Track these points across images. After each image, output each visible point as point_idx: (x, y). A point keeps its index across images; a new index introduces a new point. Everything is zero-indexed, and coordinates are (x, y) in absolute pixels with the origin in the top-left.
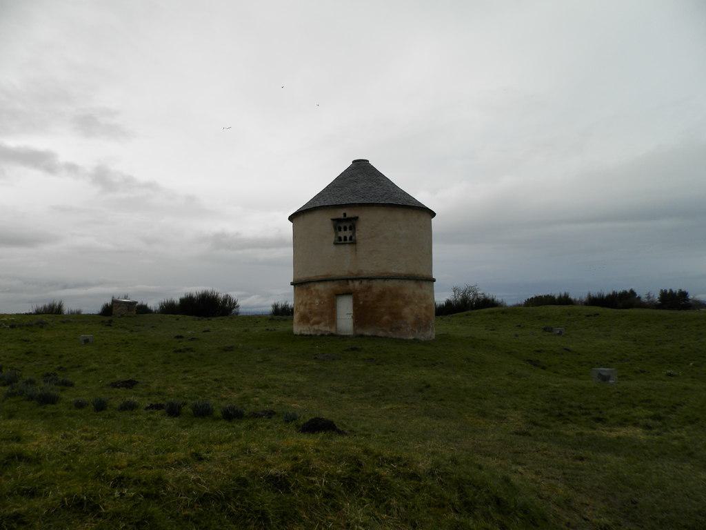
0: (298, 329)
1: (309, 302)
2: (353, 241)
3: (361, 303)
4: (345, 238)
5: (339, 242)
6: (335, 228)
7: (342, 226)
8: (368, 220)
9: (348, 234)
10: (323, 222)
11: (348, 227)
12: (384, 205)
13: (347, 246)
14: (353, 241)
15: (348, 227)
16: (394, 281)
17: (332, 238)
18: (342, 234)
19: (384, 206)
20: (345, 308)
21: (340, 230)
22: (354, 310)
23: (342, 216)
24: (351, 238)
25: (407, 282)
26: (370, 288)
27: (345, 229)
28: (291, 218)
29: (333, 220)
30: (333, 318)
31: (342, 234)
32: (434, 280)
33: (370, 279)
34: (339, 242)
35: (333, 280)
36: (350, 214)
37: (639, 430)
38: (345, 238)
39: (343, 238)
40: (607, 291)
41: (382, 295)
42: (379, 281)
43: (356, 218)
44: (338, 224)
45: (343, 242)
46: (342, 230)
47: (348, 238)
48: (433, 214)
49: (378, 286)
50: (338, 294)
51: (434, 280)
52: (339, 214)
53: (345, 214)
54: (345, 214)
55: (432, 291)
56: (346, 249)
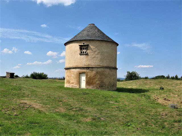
0: (66, 85)
1: (70, 75)
3: (89, 76)
5: (81, 54)
6: (80, 48)
7: (83, 48)
9: (85, 51)
10: (76, 46)
11: (85, 48)
12: (106, 41)
15: (85, 48)
16: (101, 69)
17: (79, 52)
20: (83, 78)
22: (86, 79)
24: (86, 52)
25: (106, 69)
27: (84, 49)
30: (79, 83)
32: (117, 69)
34: (81, 54)
35: (101, 68)
37: (102, 122)
40: (54, 77)
43: (88, 45)
44: (81, 47)
45: (83, 53)
46: (83, 49)
47: (85, 52)
48: (118, 45)
50: (80, 74)
51: (117, 69)
54: (84, 44)
55: (116, 73)
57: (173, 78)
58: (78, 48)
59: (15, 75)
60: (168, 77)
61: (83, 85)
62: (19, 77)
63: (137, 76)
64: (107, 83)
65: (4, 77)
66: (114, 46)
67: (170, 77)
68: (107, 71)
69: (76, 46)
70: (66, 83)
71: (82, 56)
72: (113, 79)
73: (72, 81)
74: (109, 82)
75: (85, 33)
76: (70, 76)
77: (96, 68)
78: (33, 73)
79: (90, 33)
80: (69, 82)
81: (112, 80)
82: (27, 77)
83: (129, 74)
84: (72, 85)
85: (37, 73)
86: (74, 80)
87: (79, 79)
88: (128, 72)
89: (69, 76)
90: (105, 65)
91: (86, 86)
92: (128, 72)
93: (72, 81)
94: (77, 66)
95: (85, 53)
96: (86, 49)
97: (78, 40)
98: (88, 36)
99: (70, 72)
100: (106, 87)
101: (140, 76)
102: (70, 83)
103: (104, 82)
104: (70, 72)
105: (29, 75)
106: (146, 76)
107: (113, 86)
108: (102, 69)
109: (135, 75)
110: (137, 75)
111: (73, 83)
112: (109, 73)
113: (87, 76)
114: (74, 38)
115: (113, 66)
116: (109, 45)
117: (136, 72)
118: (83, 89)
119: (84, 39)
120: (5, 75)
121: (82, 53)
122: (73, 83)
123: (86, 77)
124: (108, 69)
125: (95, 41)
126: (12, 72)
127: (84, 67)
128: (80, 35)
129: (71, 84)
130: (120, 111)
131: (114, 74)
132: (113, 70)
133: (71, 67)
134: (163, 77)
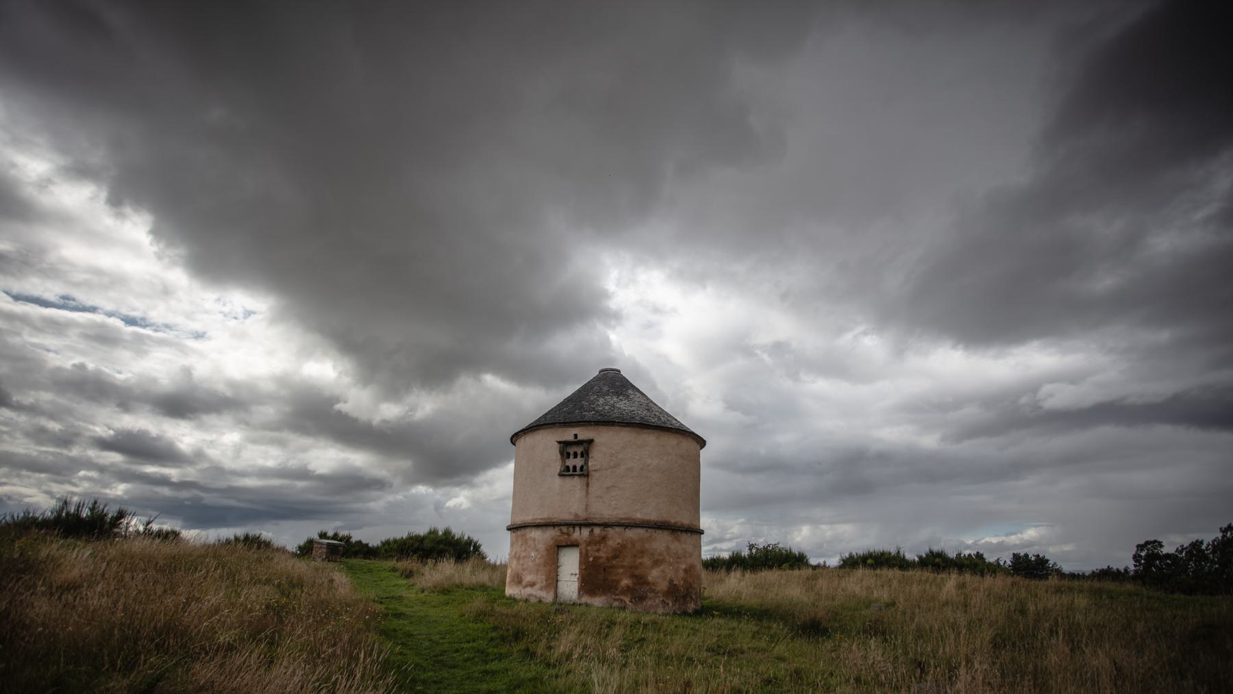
1: (523, 554)
2: (584, 473)
4: (575, 467)
5: (566, 472)
6: (562, 453)
7: (571, 450)
8: (608, 444)
9: (579, 462)
10: (548, 442)
14: (584, 473)
17: (557, 467)
18: (571, 462)
19: (595, 521)
20: (570, 563)
21: (568, 455)
23: (571, 438)
24: (582, 468)
25: (659, 532)
26: (604, 539)
27: (575, 455)
28: (512, 528)
29: (559, 442)
30: (553, 581)
31: (571, 462)
32: (702, 532)
33: (605, 525)
34: (566, 472)
36: (583, 434)
38: (575, 467)
41: (618, 553)
42: (618, 529)
43: (591, 442)
44: (565, 448)
48: (702, 443)
49: (615, 537)
51: (702, 532)
52: (568, 434)
53: (576, 436)
54: (576, 436)
56: (576, 483)
58: (554, 452)
61: (569, 585)
64: (663, 586)
66: (687, 444)
68: (661, 541)
69: (548, 442)
71: (568, 480)
73: (528, 578)
74: (671, 581)
77: (619, 525)
80: (518, 580)
84: (529, 590)
89: (519, 559)
90: (653, 516)
93: (528, 578)
99: (526, 542)
103: (648, 584)
104: (526, 542)
108: (640, 532)
111: (532, 585)
112: (668, 547)
122: (532, 585)
124: (666, 533)
125: (616, 428)
130: (655, 623)
131: (690, 548)
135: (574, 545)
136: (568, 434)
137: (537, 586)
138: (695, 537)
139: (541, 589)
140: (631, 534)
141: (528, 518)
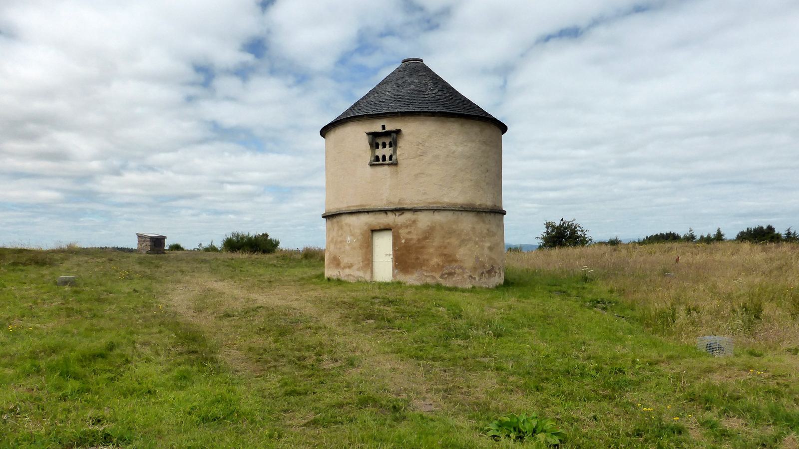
1: (339, 239)
3: (403, 241)
4: (384, 157)
5: (376, 162)
6: (371, 145)
7: (380, 141)
9: (387, 151)
10: (356, 136)
11: (387, 143)
13: (386, 167)
15: (387, 143)
17: (368, 157)
18: (380, 152)
20: (384, 245)
22: (394, 250)
24: (391, 157)
27: (384, 146)
29: (368, 134)
30: (368, 262)
31: (380, 152)
32: (504, 213)
33: (414, 210)
34: (376, 162)
36: (390, 126)
38: (384, 157)
39: (380, 147)
41: (428, 234)
43: (398, 132)
44: (375, 139)
45: (381, 162)
46: (380, 147)
47: (387, 158)
48: (503, 128)
51: (504, 213)
52: (377, 127)
53: (384, 127)
54: (384, 127)
55: (501, 226)
57: (708, 240)
58: (364, 142)
59: (168, 243)
60: (690, 238)
61: (384, 267)
62: (182, 249)
63: (579, 237)
65: (131, 251)
67: (698, 238)
68: (467, 222)
69: (356, 136)
70: (329, 264)
72: (491, 249)
75: (389, 91)
76: (341, 242)
78: (230, 236)
79: (406, 89)
81: (486, 251)
82: (212, 249)
83: (553, 231)
85: (238, 235)
86: (352, 256)
87: (426, 210)
88: (548, 225)
89: (336, 243)
91: (394, 276)
92: (548, 225)
93: (345, 260)
94: (361, 206)
95: (387, 162)
96: (391, 146)
97: (363, 116)
98: (398, 99)
100: (465, 276)
101: (588, 235)
102: (342, 265)
103: (456, 261)
105: (219, 244)
106: (614, 238)
107: (489, 272)
109: (574, 232)
110: (579, 233)
113: (396, 239)
114: (352, 109)
115: (488, 202)
116: (474, 129)
117: (575, 223)
118: (382, 285)
119: (385, 111)
120: (133, 244)
121: (379, 161)
123: (394, 244)
126: (153, 232)
127: (386, 207)
128: (371, 99)
129: (345, 268)
131: (494, 228)
132: (489, 218)
133: (344, 210)
134: (671, 237)
135: (386, 229)
136: (377, 127)
137: (355, 267)
138: (498, 216)
139: (358, 270)
140: (439, 217)
141: (343, 206)
